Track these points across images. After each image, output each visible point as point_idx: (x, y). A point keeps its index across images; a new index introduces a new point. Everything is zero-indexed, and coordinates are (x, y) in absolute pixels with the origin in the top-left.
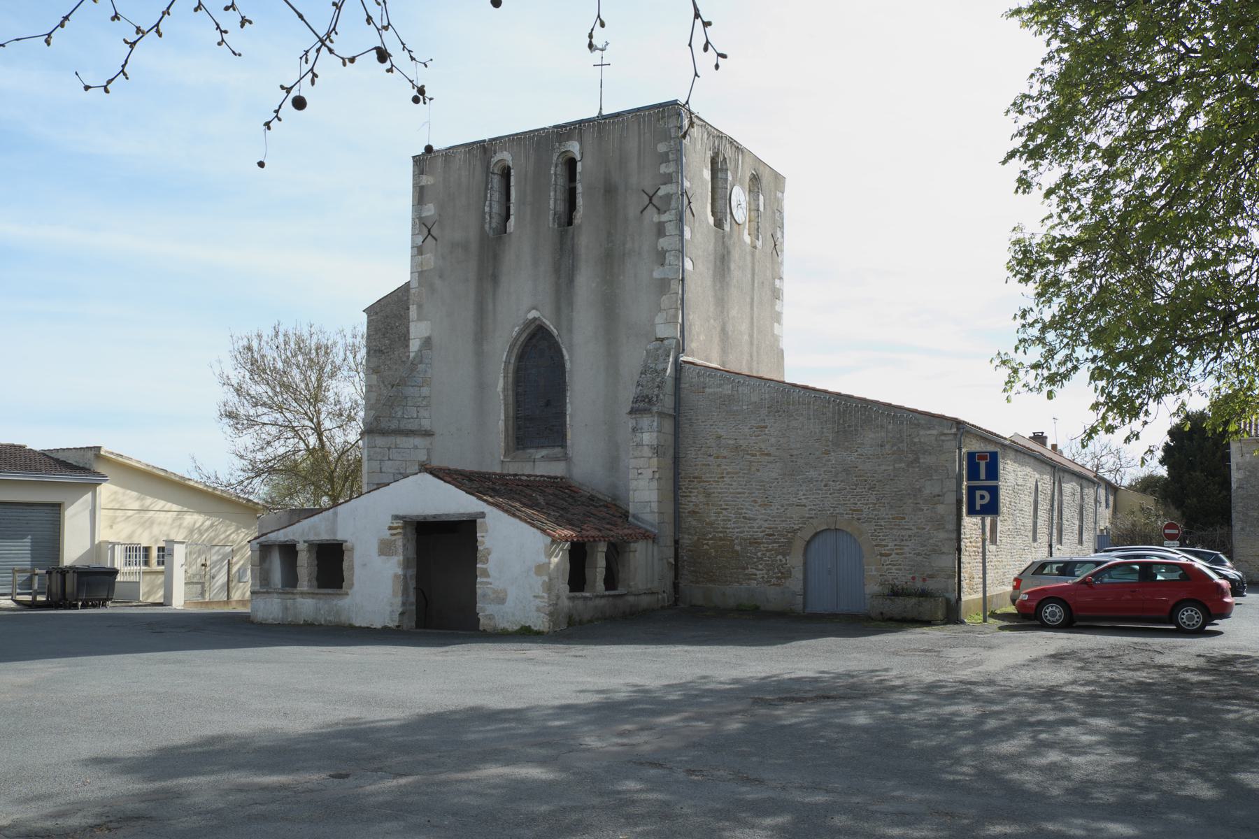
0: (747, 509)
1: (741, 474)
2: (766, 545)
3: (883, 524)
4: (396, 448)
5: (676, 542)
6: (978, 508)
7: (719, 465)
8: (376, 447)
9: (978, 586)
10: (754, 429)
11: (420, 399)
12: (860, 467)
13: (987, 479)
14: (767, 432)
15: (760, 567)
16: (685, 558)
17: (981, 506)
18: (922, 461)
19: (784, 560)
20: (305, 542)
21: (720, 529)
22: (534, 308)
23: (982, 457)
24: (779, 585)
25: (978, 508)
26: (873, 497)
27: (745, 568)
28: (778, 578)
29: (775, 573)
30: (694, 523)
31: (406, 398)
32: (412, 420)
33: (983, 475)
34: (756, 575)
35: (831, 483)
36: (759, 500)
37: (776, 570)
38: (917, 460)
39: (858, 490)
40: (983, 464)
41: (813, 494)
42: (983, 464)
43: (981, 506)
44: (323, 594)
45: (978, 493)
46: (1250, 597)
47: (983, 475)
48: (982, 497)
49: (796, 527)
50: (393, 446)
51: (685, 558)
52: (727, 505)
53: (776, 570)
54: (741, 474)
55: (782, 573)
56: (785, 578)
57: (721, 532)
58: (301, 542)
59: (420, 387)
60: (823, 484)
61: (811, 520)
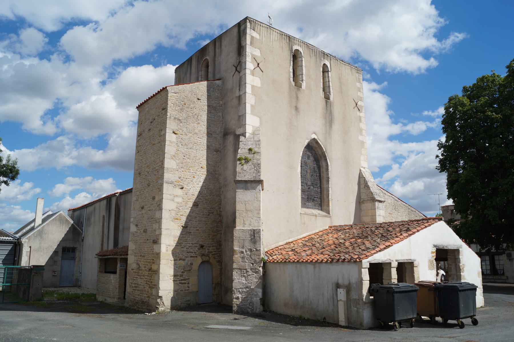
20: (396, 261)
22: (315, 133)
58: (395, 261)
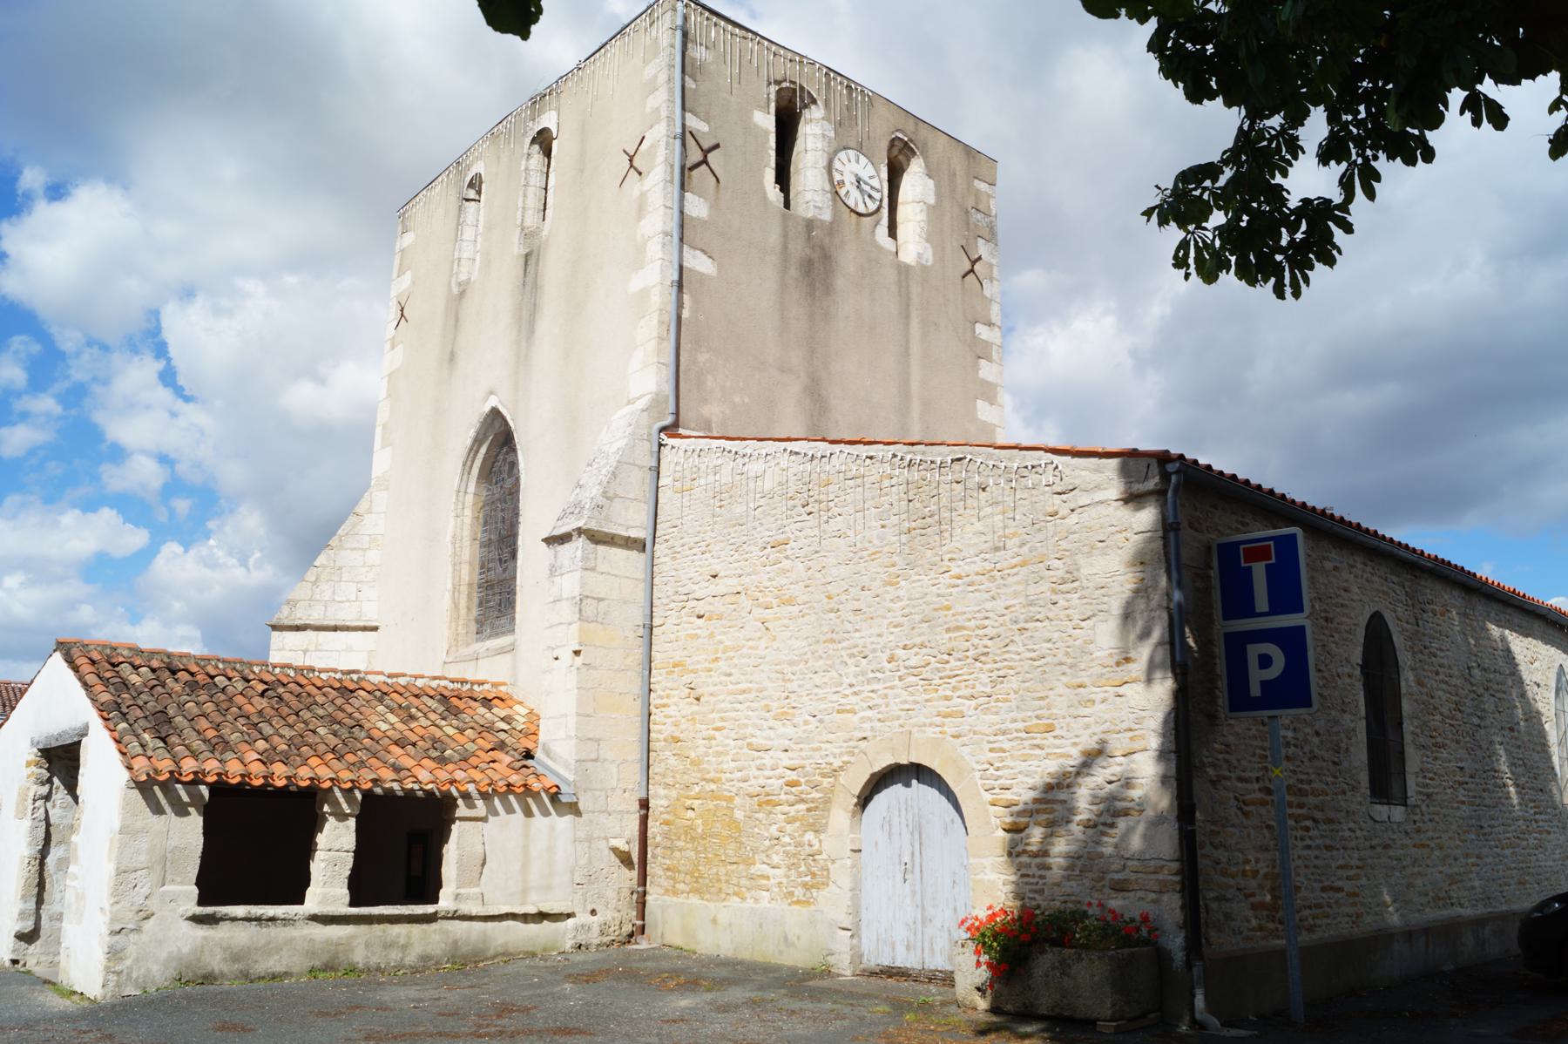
0: (754, 725)
1: (745, 651)
2: (786, 808)
3: (1006, 745)
4: (317, 650)
5: (644, 804)
6: (1255, 691)
7: (711, 635)
8: (283, 649)
9: (833, 902)
10: (769, 549)
11: (364, 570)
12: (959, 608)
13: (1275, 610)
14: (789, 552)
15: (776, 859)
16: (658, 839)
17: (1264, 684)
18: (1085, 571)
19: (815, 842)
21: (712, 775)
23: (1258, 553)
24: (807, 903)
25: (1255, 691)
26: (984, 678)
27: (749, 863)
28: (805, 885)
29: (800, 875)
30: (673, 761)
31: (340, 568)
32: (348, 604)
33: (1262, 601)
34: (768, 878)
35: (900, 652)
36: (774, 705)
37: (803, 868)
38: (1072, 577)
39: (953, 663)
40: (1259, 570)
41: (869, 681)
42: (1259, 570)
43: (1264, 684)
44: (248, 919)
45: (1254, 651)
46: (7, 958)
47: (1262, 601)
48: (1265, 661)
49: (837, 763)
50: (312, 647)
51: (658, 839)
52: (723, 719)
53: (803, 868)
54: (745, 651)
55: (814, 875)
56: (816, 886)
57: (713, 781)
59: (365, 550)
60: (885, 657)
61: (863, 744)
